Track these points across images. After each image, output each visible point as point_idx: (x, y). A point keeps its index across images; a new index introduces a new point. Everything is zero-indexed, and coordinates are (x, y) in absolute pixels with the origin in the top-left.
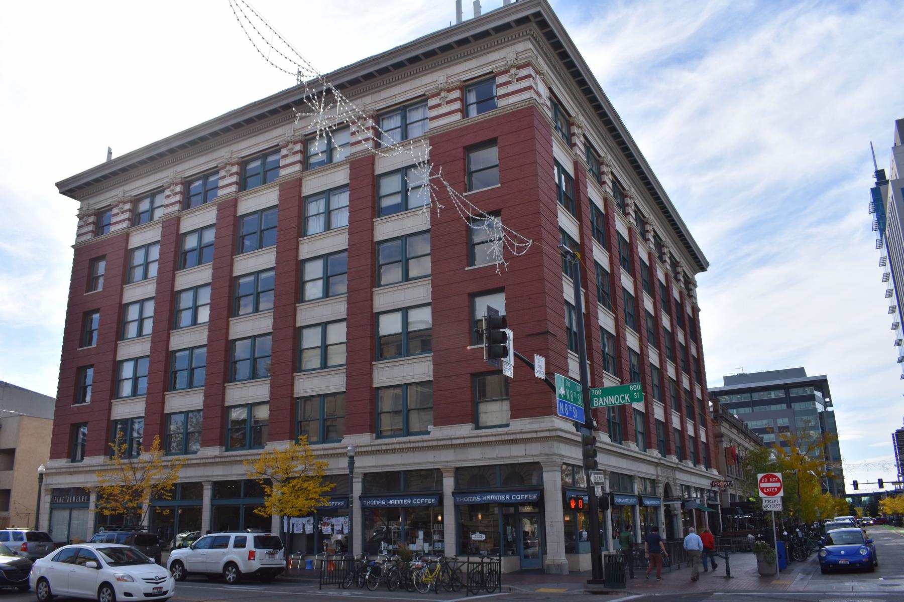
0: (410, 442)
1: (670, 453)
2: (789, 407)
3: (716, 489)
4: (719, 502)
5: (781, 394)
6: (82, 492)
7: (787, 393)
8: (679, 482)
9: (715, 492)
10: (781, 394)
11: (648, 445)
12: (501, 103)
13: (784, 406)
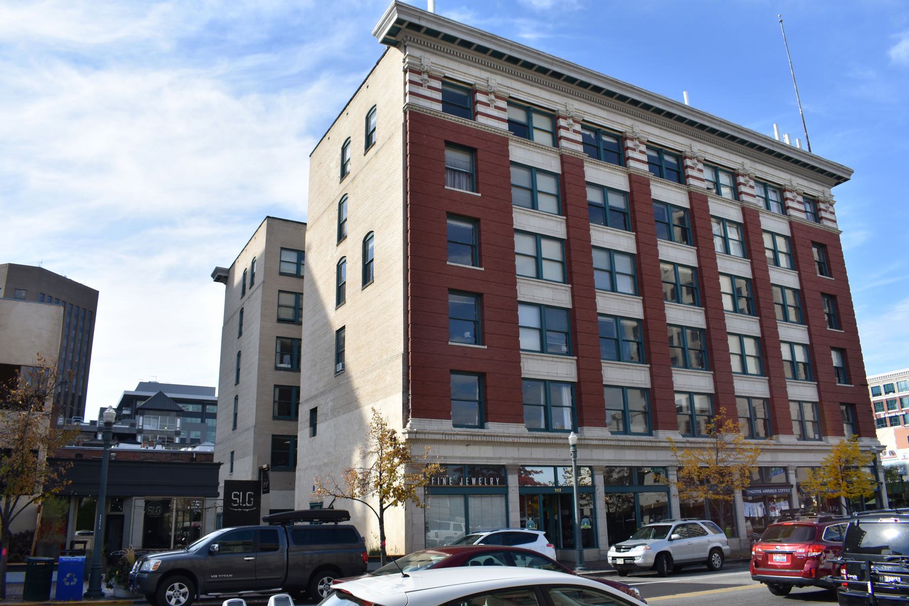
2: (203, 421)
5: (197, 408)
6: (499, 472)
7: (204, 408)
10: (197, 408)
12: (480, 119)
13: (199, 420)
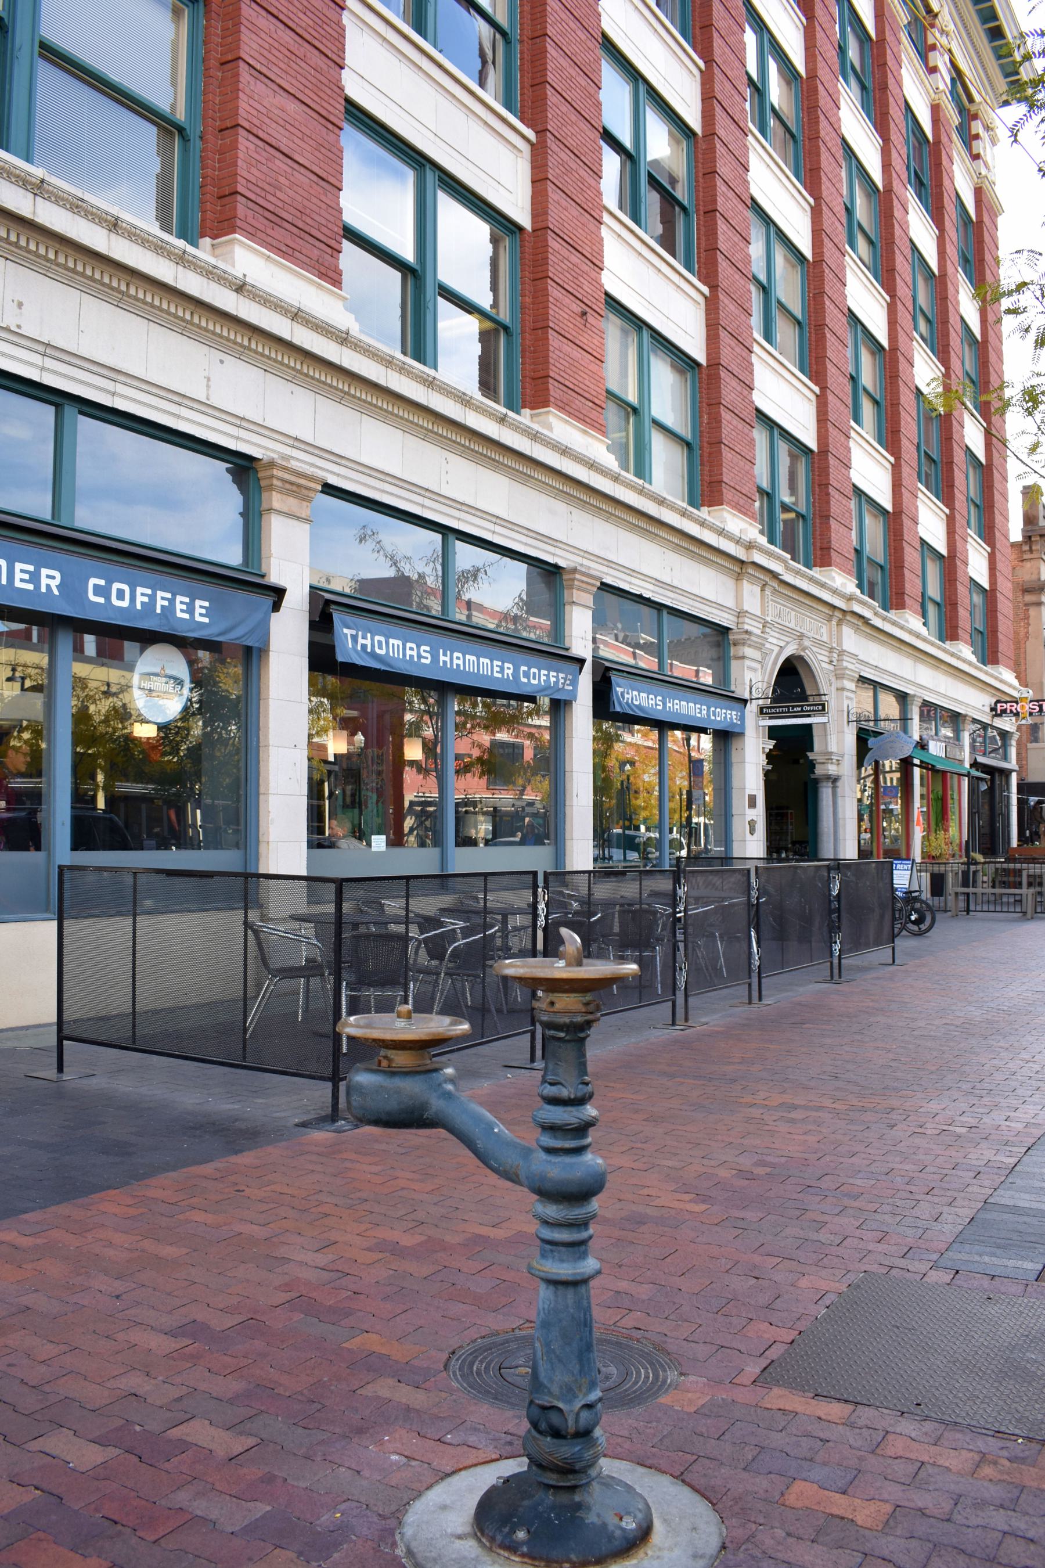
0: (423, 506)
1: (900, 605)
3: (1007, 724)
4: (1013, 764)
8: (852, 667)
9: (1004, 735)
11: (949, 632)
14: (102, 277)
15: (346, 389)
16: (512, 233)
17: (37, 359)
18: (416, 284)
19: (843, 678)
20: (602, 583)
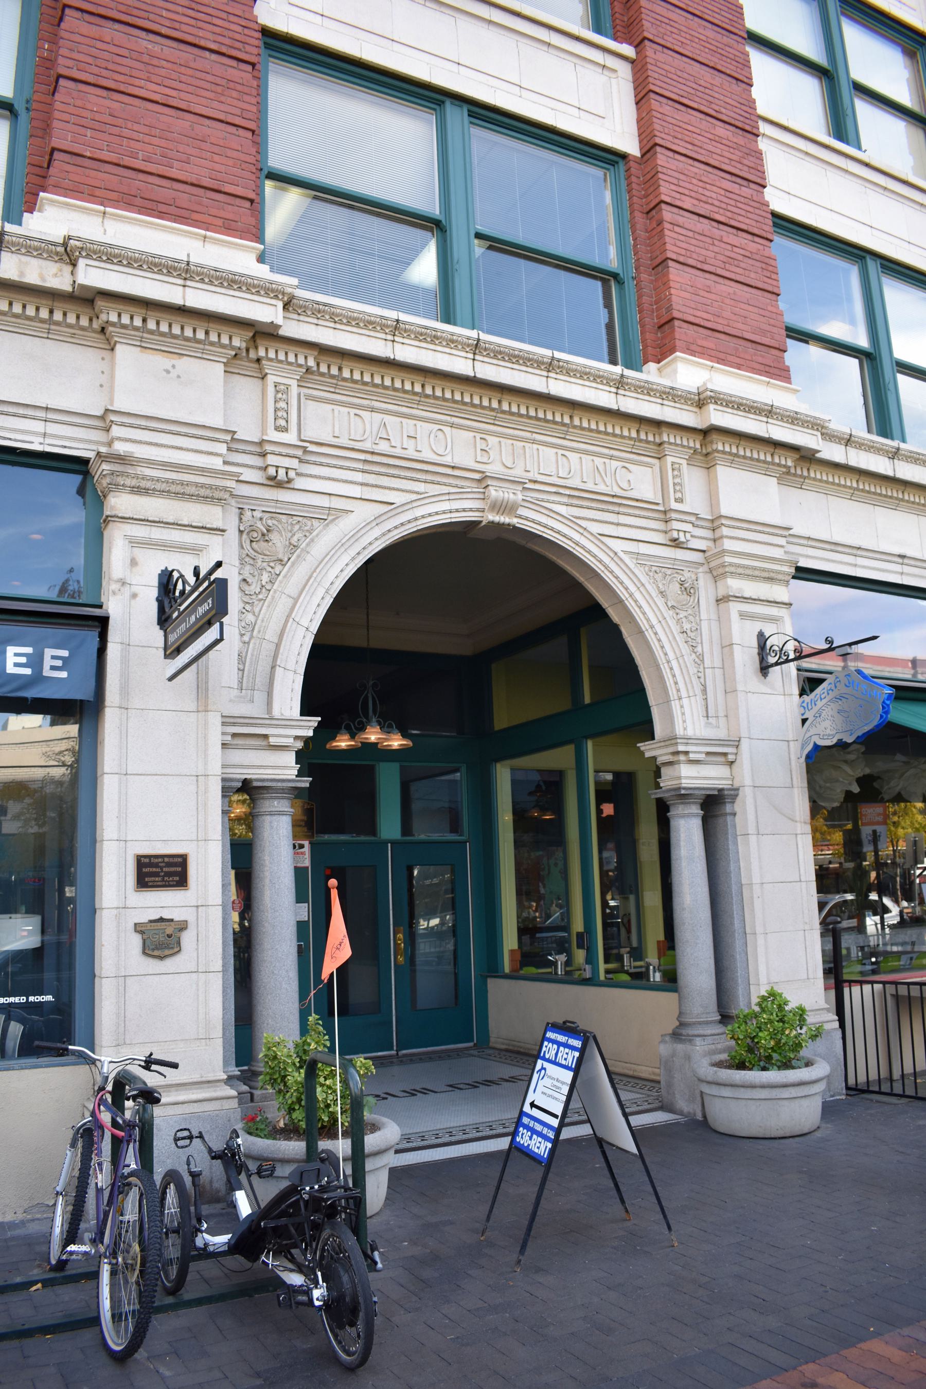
14: (581, 422)
15: (900, 496)
16: (613, 164)
17: (898, 568)
18: (872, 365)
19: (724, 575)
20: (799, 569)
